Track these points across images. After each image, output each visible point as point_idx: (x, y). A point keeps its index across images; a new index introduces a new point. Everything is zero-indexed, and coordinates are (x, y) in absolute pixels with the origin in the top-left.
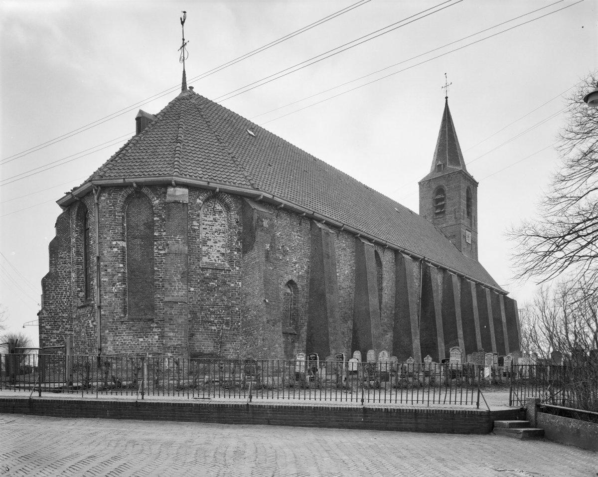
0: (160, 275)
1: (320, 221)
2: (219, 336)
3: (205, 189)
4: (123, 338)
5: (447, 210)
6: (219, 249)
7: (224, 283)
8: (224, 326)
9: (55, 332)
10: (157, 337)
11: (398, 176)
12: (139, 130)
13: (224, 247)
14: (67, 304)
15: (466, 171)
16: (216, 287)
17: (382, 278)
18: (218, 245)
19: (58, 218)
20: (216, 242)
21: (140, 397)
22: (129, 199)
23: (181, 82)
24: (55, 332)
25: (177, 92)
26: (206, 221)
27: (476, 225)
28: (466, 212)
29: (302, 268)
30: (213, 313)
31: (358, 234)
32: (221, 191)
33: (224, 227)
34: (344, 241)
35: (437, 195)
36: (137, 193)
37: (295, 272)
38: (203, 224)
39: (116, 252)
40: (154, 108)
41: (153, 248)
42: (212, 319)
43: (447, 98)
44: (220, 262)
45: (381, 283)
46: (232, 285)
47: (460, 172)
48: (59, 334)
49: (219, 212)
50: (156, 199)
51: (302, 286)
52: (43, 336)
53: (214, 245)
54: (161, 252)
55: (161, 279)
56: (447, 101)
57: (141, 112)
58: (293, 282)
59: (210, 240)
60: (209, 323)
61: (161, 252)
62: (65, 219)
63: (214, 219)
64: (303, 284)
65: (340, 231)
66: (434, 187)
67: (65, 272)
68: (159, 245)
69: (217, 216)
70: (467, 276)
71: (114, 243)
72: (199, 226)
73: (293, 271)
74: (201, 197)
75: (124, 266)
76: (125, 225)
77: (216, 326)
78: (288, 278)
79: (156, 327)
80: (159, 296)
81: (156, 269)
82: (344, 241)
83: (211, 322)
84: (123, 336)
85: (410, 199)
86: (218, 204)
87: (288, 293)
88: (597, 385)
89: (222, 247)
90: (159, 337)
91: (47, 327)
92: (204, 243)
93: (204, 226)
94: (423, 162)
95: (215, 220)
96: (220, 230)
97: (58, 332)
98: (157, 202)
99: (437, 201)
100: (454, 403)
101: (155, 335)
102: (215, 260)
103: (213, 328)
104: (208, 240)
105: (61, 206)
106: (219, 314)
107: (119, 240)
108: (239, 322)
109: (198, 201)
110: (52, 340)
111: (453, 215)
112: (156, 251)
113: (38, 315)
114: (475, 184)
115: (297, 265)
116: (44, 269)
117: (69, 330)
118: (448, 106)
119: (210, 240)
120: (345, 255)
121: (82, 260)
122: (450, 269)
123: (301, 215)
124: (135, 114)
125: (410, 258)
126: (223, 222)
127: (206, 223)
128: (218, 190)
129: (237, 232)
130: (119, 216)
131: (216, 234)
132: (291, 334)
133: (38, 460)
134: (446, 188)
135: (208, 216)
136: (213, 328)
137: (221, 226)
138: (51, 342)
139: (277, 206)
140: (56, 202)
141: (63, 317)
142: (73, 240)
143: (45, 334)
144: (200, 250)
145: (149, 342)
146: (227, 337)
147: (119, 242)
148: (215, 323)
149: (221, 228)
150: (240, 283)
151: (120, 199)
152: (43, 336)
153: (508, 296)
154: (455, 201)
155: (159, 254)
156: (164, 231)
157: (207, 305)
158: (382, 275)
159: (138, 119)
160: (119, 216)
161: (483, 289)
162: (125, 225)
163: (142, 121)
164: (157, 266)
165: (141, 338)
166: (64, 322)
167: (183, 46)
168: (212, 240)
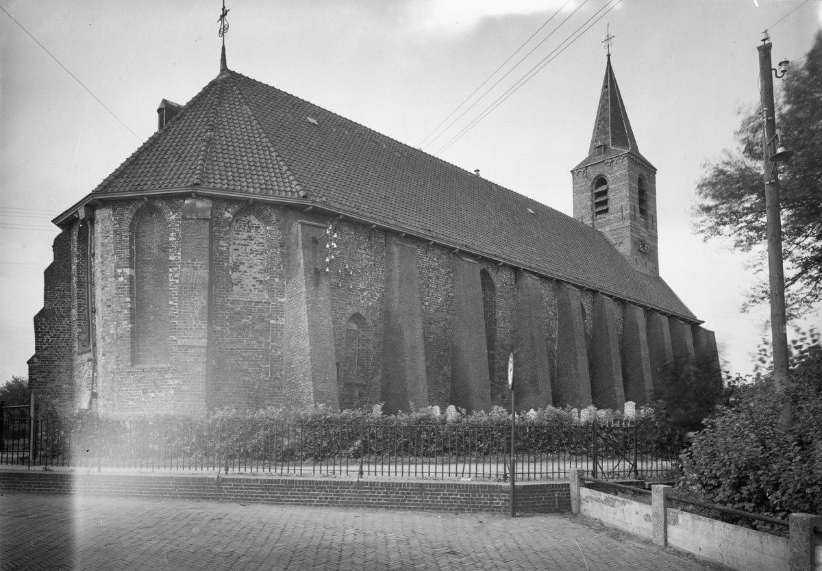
2: (254, 388)
4: (129, 393)
6: (254, 275)
7: (262, 319)
10: (172, 391)
11: (539, 162)
13: (261, 273)
16: (250, 325)
18: (253, 270)
19: (56, 239)
20: (251, 267)
21: (223, 471)
22: (139, 213)
23: (220, 58)
25: (214, 73)
26: (238, 240)
28: (638, 210)
29: (373, 296)
30: (246, 359)
33: (263, 246)
37: (362, 302)
38: (234, 244)
39: (122, 282)
40: (182, 98)
41: (167, 277)
42: (245, 367)
43: (609, 56)
44: (256, 292)
46: (272, 322)
49: (256, 227)
50: (171, 213)
51: (373, 321)
53: (248, 270)
56: (609, 59)
57: (165, 101)
59: (243, 264)
60: (240, 371)
62: (65, 241)
63: (248, 237)
64: (375, 318)
69: (253, 233)
71: (119, 271)
72: (228, 248)
73: (359, 301)
74: (230, 210)
75: (132, 300)
76: (134, 247)
80: (175, 338)
81: (171, 303)
87: (354, 331)
88: (821, 455)
89: (259, 273)
90: (175, 391)
91: (38, 380)
92: (235, 268)
93: (235, 247)
94: (577, 138)
95: (250, 238)
96: (257, 251)
98: (173, 217)
99: (599, 195)
100: (468, 475)
102: (251, 290)
104: (241, 263)
106: (254, 361)
107: (126, 267)
108: (281, 370)
109: (227, 215)
111: (620, 213)
112: (171, 280)
113: (28, 363)
114: (652, 170)
115: (365, 293)
116: (39, 304)
118: (610, 66)
119: (243, 264)
120: (437, 278)
121: (83, 293)
123: (370, 228)
124: (158, 105)
126: (261, 240)
127: (237, 242)
129: (278, 253)
130: (126, 237)
131: (251, 256)
132: (358, 385)
133: (41, 562)
134: (609, 178)
135: (241, 233)
137: (258, 246)
140: (53, 221)
142: (74, 267)
143: (35, 388)
144: (229, 279)
145: (163, 397)
148: (249, 372)
149: (258, 248)
151: (128, 216)
153: (702, 325)
155: (174, 284)
157: (238, 349)
160: (126, 237)
162: (134, 247)
163: (168, 112)
164: (172, 300)
165: (153, 392)
166: (61, 373)
168: (246, 265)
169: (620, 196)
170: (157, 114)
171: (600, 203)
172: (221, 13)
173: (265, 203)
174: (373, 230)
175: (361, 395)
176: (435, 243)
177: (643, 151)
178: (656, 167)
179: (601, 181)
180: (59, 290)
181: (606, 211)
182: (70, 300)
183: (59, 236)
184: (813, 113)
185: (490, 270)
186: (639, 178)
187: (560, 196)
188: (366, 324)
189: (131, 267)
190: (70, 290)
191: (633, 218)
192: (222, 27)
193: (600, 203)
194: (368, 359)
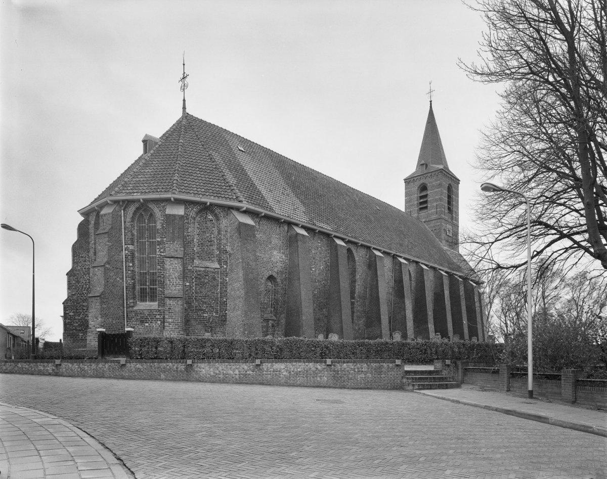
1: (297, 225)
5: (429, 205)
9: (77, 317)
10: (159, 322)
12: (145, 151)
15: (448, 169)
17: (355, 271)
24: (77, 317)
25: (176, 115)
27: (457, 220)
32: (211, 204)
35: (421, 192)
36: (143, 209)
43: (431, 101)
45: (354, 276)
47: (441, 171)
48: (80, 320)
52: (67, 321)
54: (163, 254)
56: (431, 104)
61: (163, 254)
65: (315, 233)
66: (418, 183)
68: (161, 248)
78: (267, 275)
79: (159, 315)
83: (203, 310)
85: (396, 197)
86: (209, 214)
88: (584, 366)
97: (80, 318)
101: (157, 321)
103: (205, 315)
105: (82, 214)
114: (457, 181)
116: (69, 266)
124: (142, 137)
128: (208, 204)
136: (205, 315)
141: (84, 306)
143: (68, 319)
146: (216, 322)
147: (129, 246)
150: (227, 279)
152: (67, 321)
154: (436, 195)
156: (165, 237)
158: (355, 269)
159: (145, 142)
161: (593, 246)
165: (147, 323)
167: (184, 78)
170: (142, 144)
171: (423, 204)
172: (182, 77)
174: (282, 223)
175: (273, 326)
176: (319, 231)
178: (458, 177)
180: (82, 257)
181: (426, 208)
183: (83, 221)
184: (577, 438)
187: (396, 197)
188: (277, 282)
192: (183, 85)
194: (278, 304)
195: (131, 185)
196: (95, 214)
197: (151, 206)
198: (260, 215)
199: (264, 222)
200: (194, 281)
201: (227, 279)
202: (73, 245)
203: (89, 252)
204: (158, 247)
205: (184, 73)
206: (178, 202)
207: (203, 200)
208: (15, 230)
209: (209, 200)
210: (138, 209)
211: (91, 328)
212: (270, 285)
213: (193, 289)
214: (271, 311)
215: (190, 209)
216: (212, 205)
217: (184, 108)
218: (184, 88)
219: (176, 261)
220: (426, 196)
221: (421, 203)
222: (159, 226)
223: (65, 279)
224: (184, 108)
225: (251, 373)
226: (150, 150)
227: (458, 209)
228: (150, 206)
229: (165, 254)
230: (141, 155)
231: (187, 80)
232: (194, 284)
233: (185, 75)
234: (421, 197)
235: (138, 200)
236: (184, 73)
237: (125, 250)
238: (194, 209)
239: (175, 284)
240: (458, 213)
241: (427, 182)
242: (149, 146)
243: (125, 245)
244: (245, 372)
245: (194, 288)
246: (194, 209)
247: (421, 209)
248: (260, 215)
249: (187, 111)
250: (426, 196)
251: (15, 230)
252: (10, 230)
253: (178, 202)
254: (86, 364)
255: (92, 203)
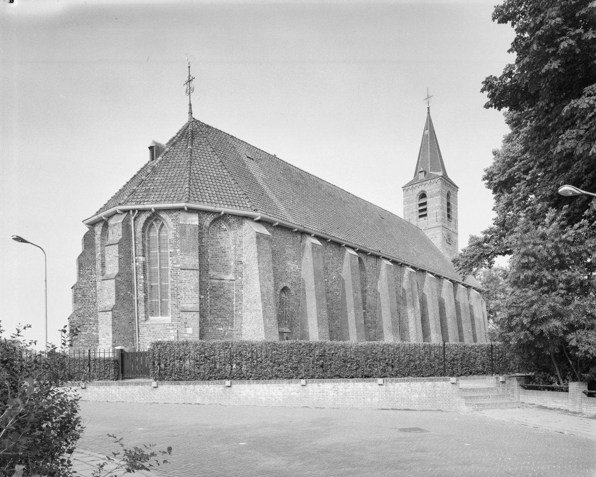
0: (174, 285)
2: (225, 335)
3: (212, 212)
8: (229, 328)
14: (94, 309)
25: (184, 120)
31: (343, 244)
32: (225, 214)
34: (331, 251)
54: (176, 266)
55: (176, 289)
58: (288, 288)
61: (176, 266)
66: (418, 191)
67: (91, 281)
70: (445, 276)
77: (223, 327)
79: (172, 329)
82: (331, 251)
84: (145, 336)
86: (223, 224)
97: (86, 333)
107: (140, 256)
110: (81, 340)
114: (456, 188)
116: (74, 279)
117: (95, 332)
122: (429, 270)
125: (391, 264)
138: (81, 342)
139: (272, 224)
147: (139, 258)
150: (242, 291)
156: (178, 248)
163: (155, 150)
166: (91, 325)
169: (435, 205)
171: (423, 212)
172: (187, 79)
173: (230, 215)
177: (450, 176)
179: (423, 196)
181: (426, 215)
182: (95, 276)
185: (363, 258)
186: (448, 194)
187: (394, 202)
189: (144, 256)
190: (95, 270)
191: (443, 220)
192: (188, 88)
193: (423, 212)
195: (140, 194)
196: (101, 224)
197: (163, 215)
198: (255, 220)
199: (279, 232)
200: (208, 293)
201: (242, 291)
202: (79, 257)
203: (95, 264)
204: (171, 258)
205: (190, 76)
206: (191, 210)
207: (218, 209)
208: (28, 242)
209: (224, 209)
210: (149, 219)
211: (101, 344)
212: (284, 296)
213: (208, 302)
214: (285, 323)
215: (204, 218)
216: (226, 214)
217: (191, 113)
218: (189, 91)
219: (192, 273)
220: (425, 204)
221: (420, 211)
222: (171, 236)
223: (70, 294)
224: (191, 113)
225: (296, 394)
226: (157, 156)
227: (457, 217)
228: (162, 216)
229: (179, 266)
230: (147, 162)
231: (193, 84)
232: (208, 297)
233: (191, 78)
234: (420, 205)
235: (150, 210)
236: (190, 76)
237: (136, 262)
238: (208, 219)
239: (190, 297)
240: (457, 220)
241: (426, 190)
242: (156, 153)
243: (136, 256)
244: (289, 394)
245: (208, 301)
246: (208, 219)
247: (420, 216)
248: (255, 220)
249: (194, 116)
250: (425, 204)
251: (28, 242)
252: (22, 241)
253: (191, 210)
254: (113, 387)
255: (97, 213)
